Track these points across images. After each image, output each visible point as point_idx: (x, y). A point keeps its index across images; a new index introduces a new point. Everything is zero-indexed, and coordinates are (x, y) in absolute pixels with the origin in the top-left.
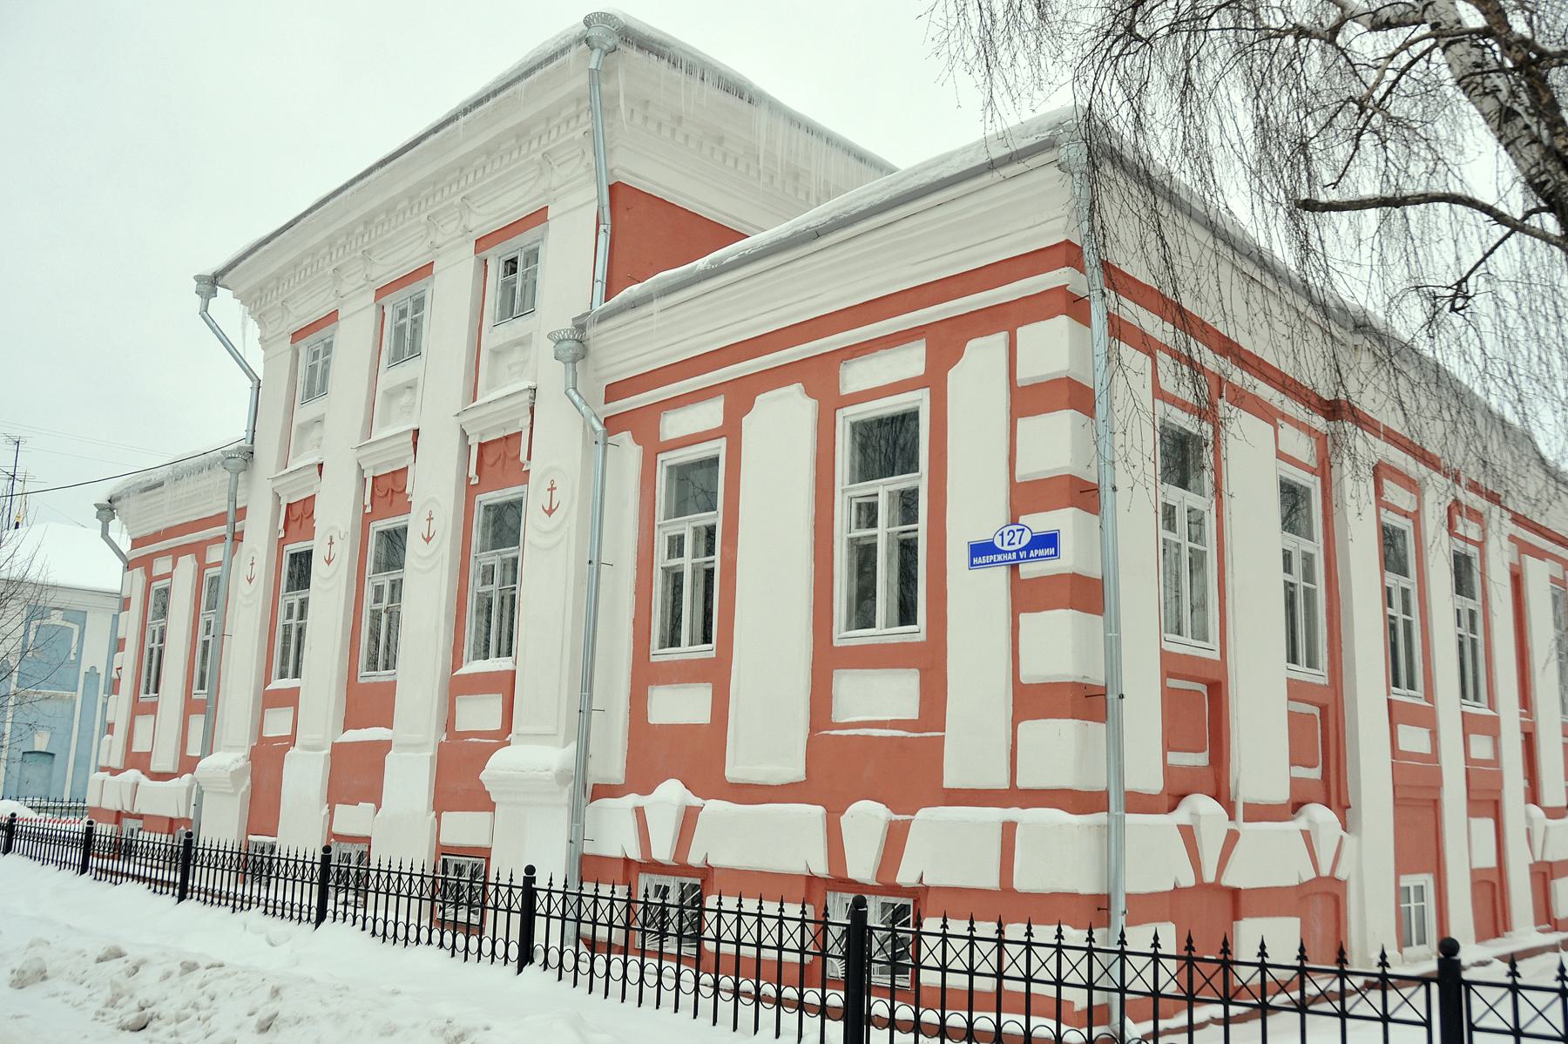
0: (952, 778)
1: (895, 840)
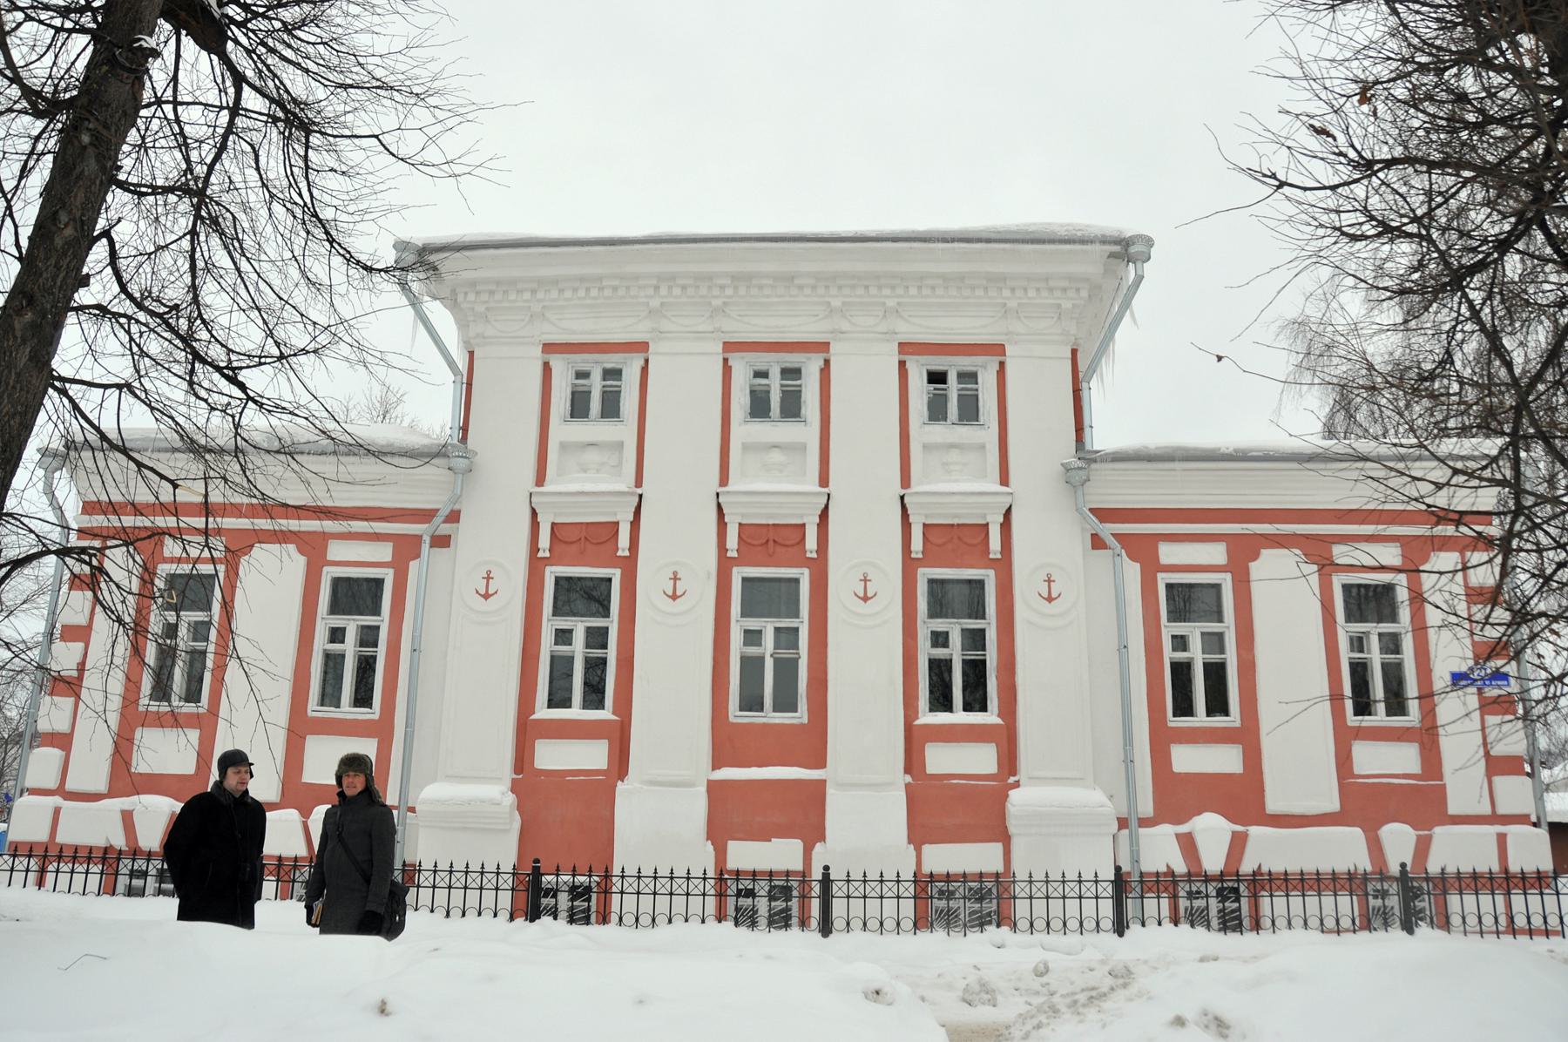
0: (1453, 809)
1: (1423, 847)
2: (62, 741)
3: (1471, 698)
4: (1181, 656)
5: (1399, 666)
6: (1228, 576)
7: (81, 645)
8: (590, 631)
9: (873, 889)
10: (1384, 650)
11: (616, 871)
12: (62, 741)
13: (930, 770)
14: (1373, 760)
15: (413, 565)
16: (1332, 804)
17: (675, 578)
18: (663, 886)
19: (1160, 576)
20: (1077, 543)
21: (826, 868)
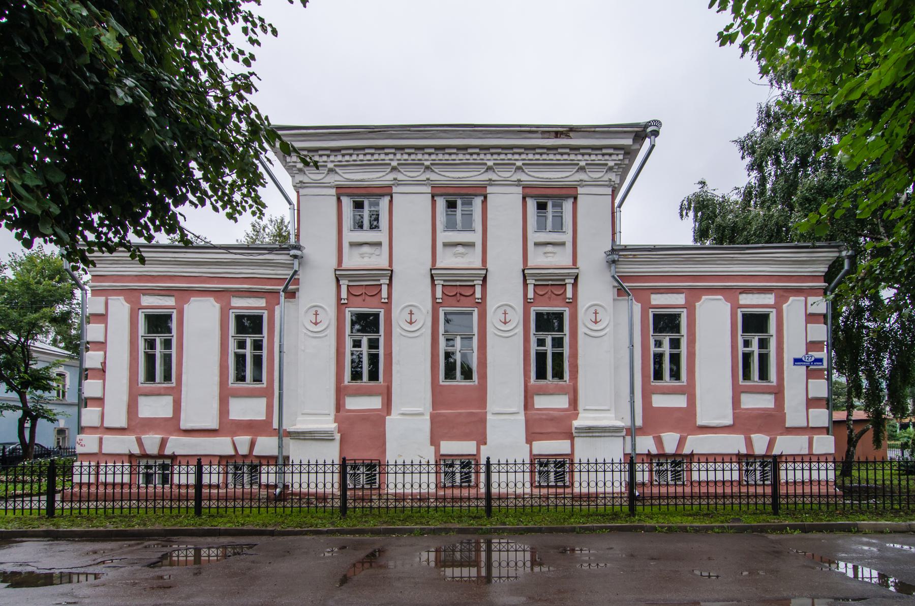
2: (100, 401)
3: (802, 369)
4: (659, 350)
5: (170, 356)
6: (266, 312)
7: (102, 353)
8: (370, 340)
9: (416, 469)
10: (370, 347)
11: (576, 460)
12: (100, 401)
13: (536, 406)
14: (750, 402)
15: (277, 307)
16: (729, 421)
17: (411, 313)
18: (600, 468)
19: (739, 310)
20: (610, 293)
21: (488, 458)
